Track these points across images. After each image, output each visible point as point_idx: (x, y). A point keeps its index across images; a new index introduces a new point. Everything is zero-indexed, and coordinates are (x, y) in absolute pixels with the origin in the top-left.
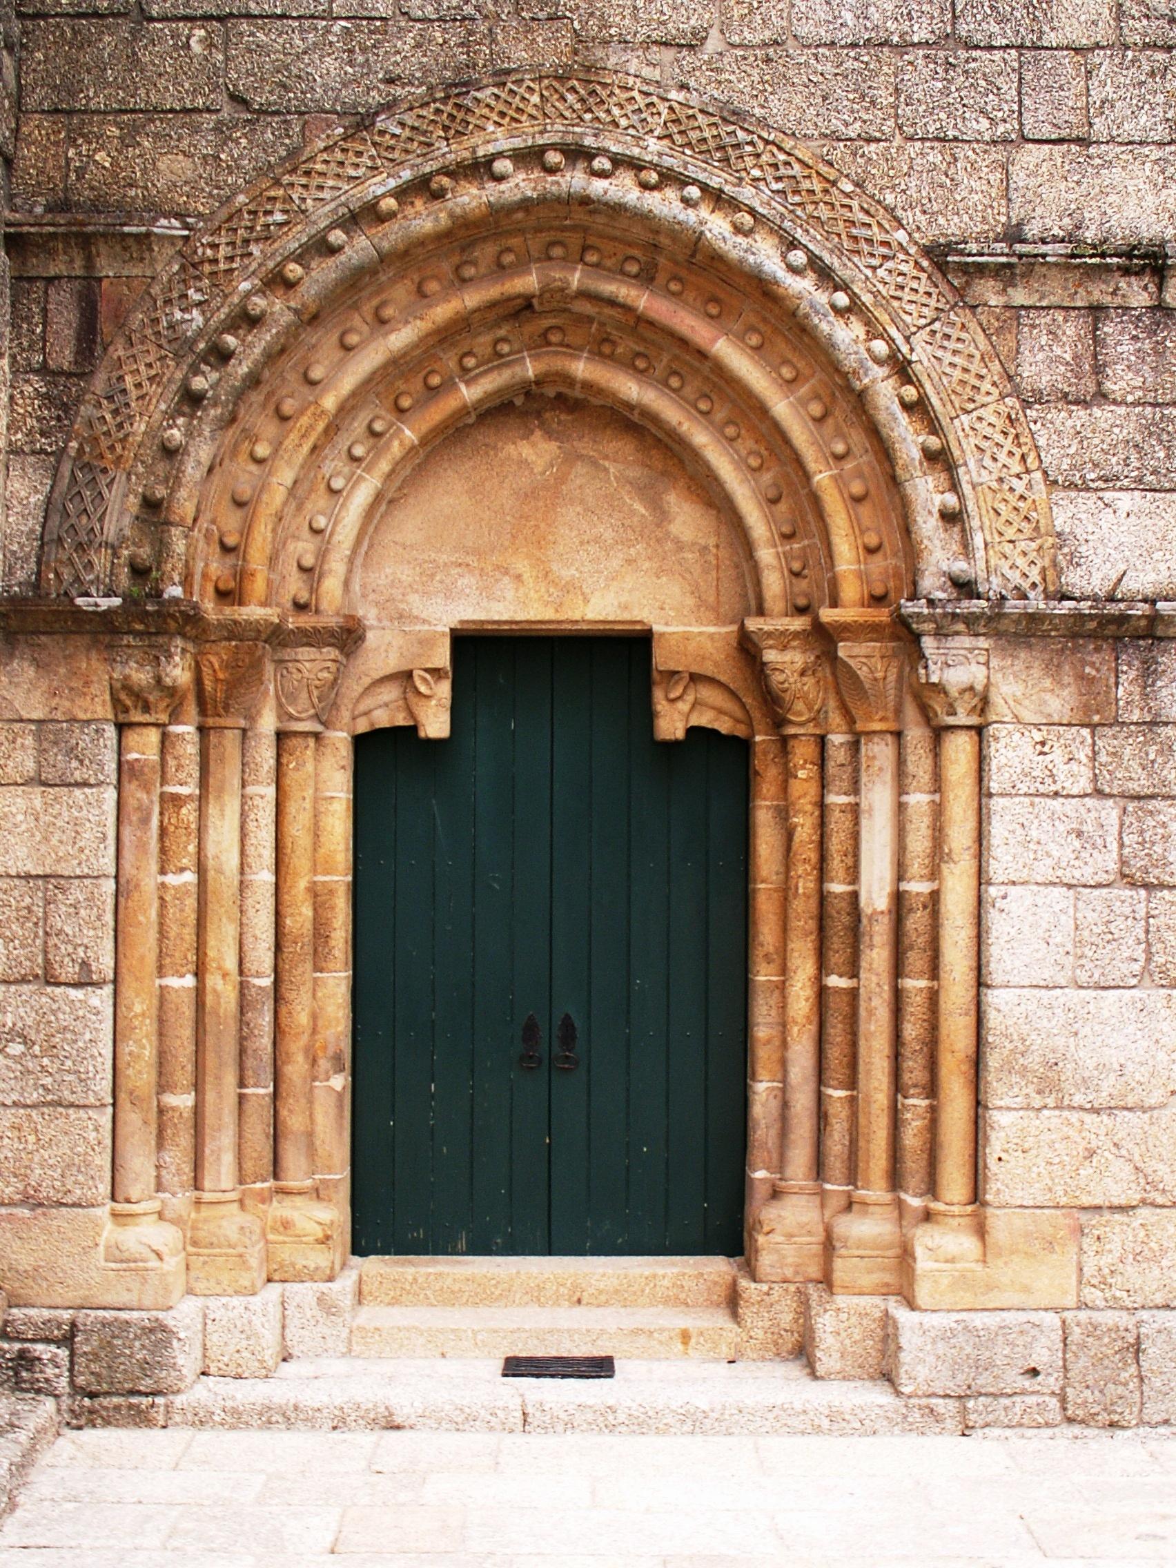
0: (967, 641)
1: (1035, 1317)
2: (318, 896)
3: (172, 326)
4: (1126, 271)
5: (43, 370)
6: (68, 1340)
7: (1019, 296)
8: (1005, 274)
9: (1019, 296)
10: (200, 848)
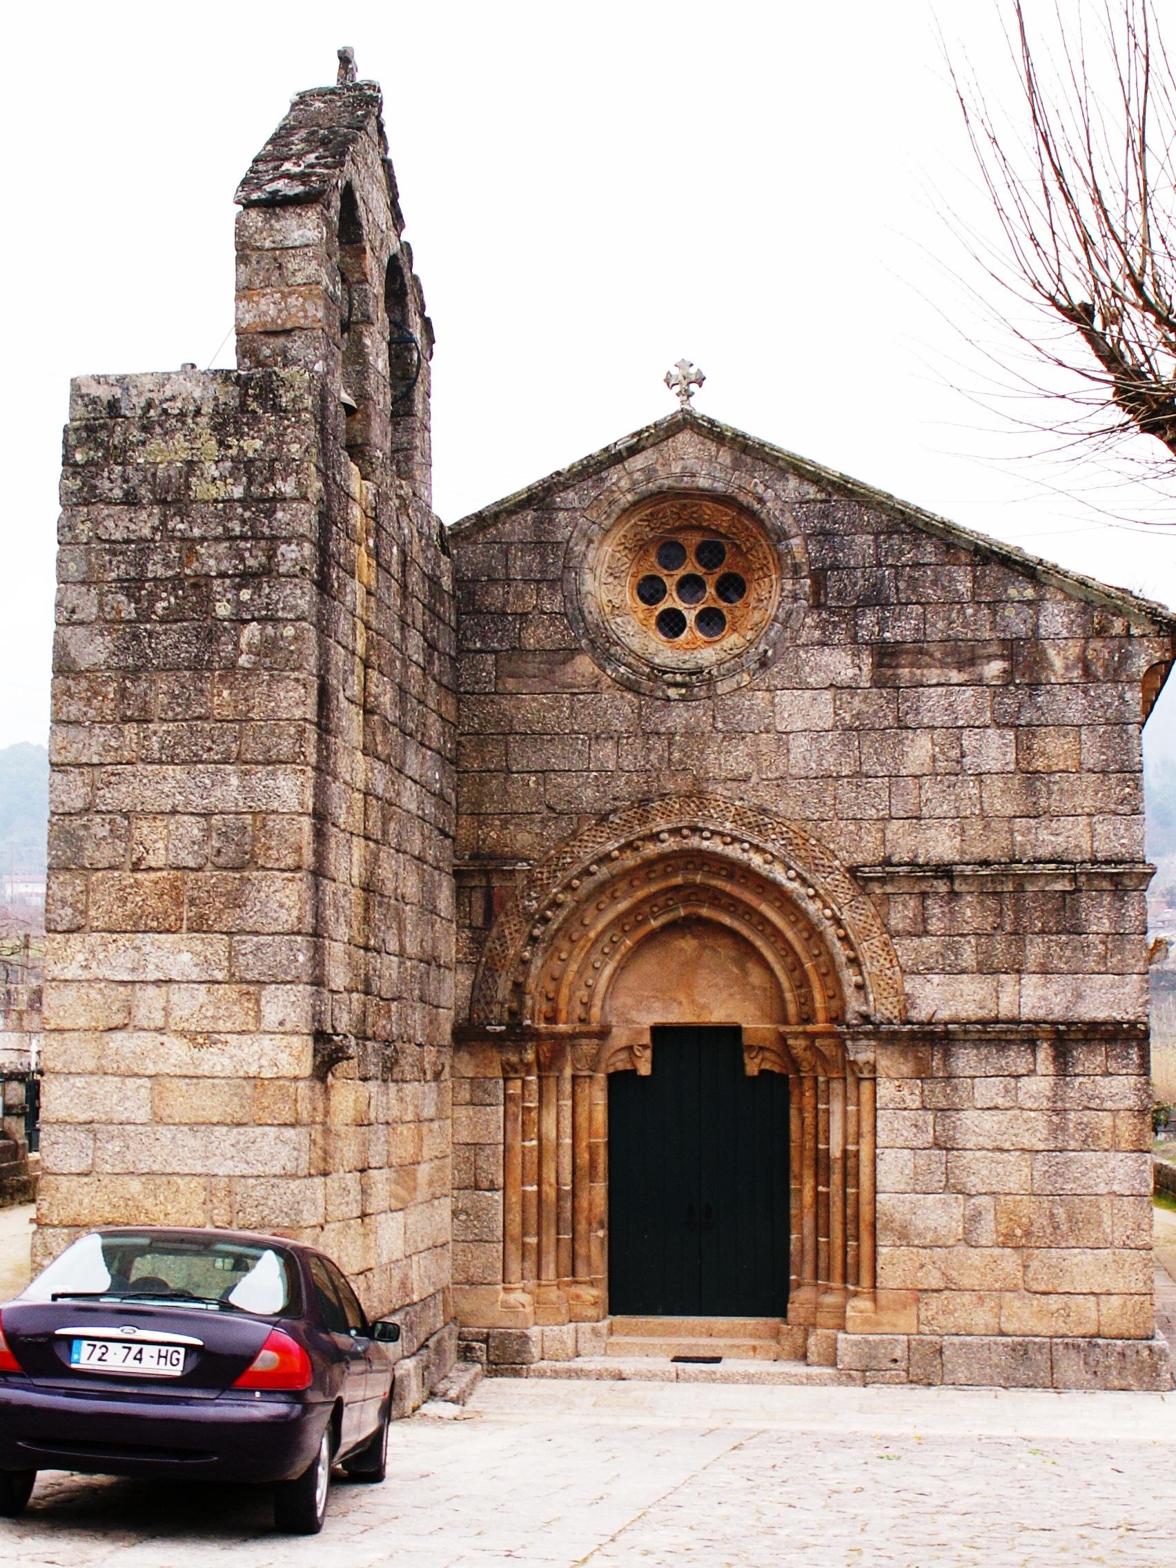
0: (865, 1042)
1: (896, 1337)
2: (591, 1148)
3: (524, 908)
4: (936, 878)
5: (470, 927)
6: (486, 1341)
7: (889, 889)
8: (882, 881)
9: (889, 889)
10: (539, 1130)
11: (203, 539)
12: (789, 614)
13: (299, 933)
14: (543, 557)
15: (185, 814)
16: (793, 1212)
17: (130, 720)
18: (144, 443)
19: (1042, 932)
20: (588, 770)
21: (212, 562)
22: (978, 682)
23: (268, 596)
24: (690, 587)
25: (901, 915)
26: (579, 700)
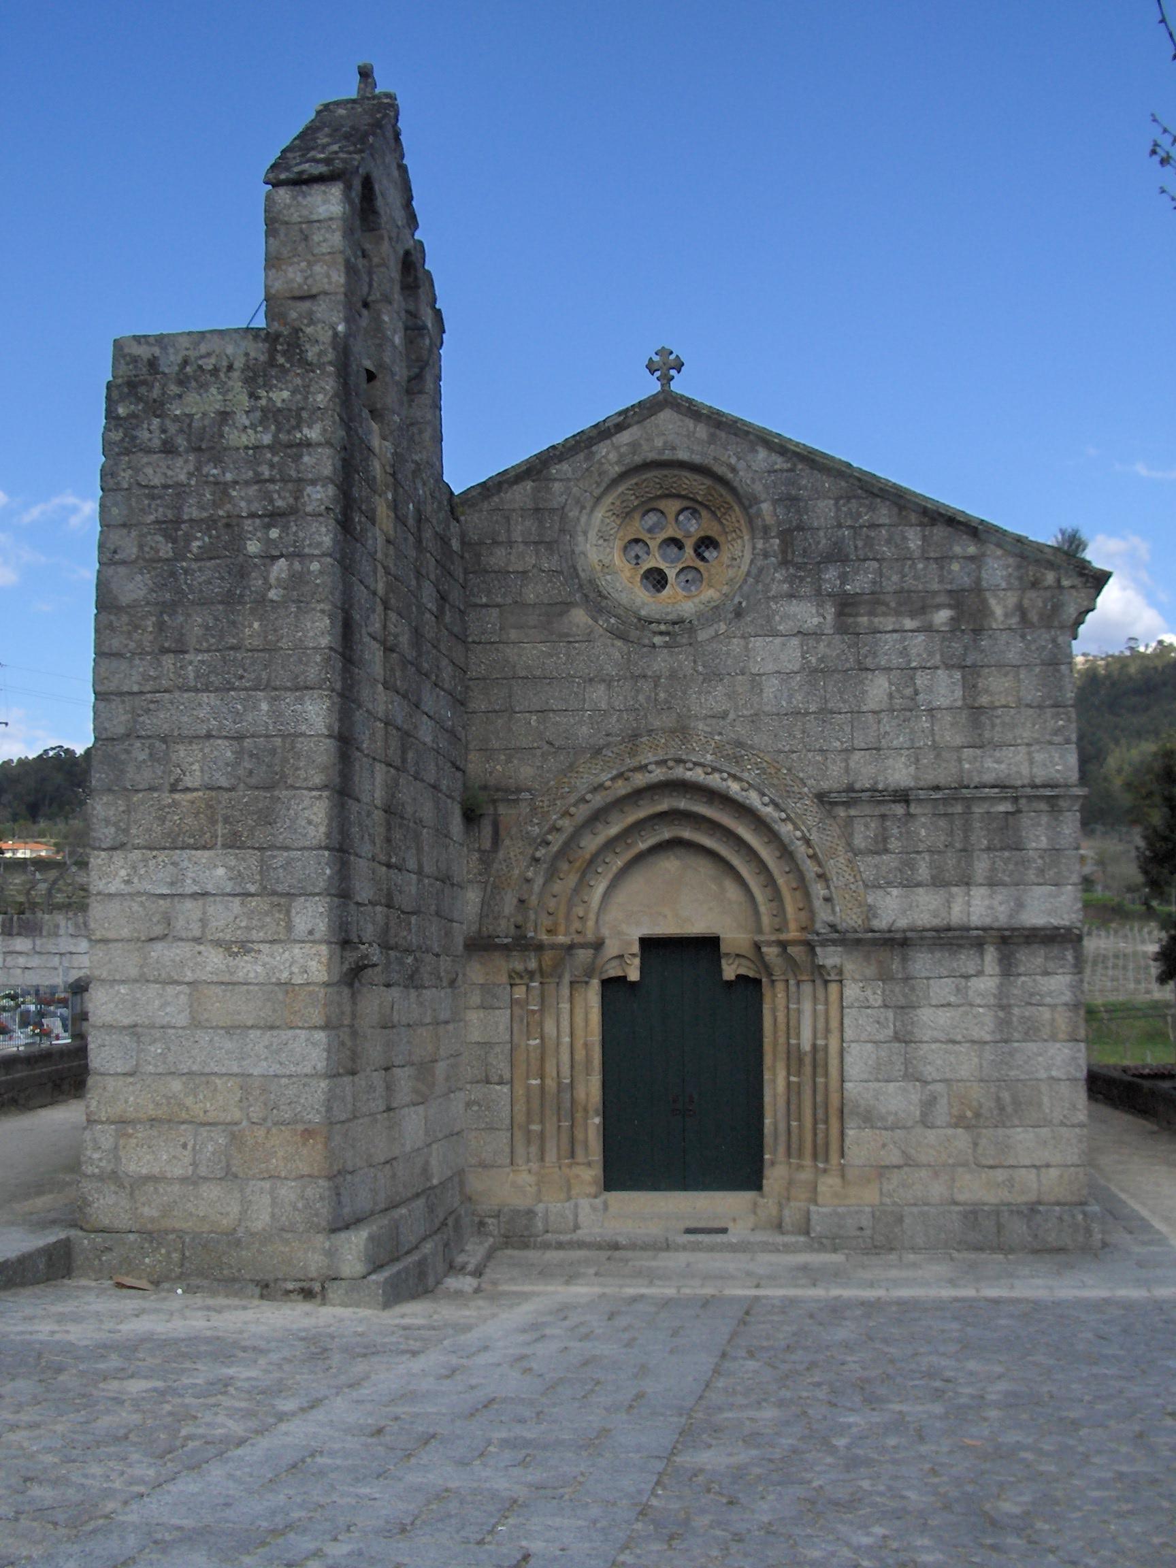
0: (832, 948)
4: (894, 802)
6: (497, 1216)
8: (847, 804)
9: (852, 812)
11: (236, 482)
12: (761, 570)
14: (541, 522)
15: (219, 738)
17: (168, 651)
19: (988, 849)
20: (583, 710)
21: (243, 504)
23: (295, 534)
26: (575, 648)
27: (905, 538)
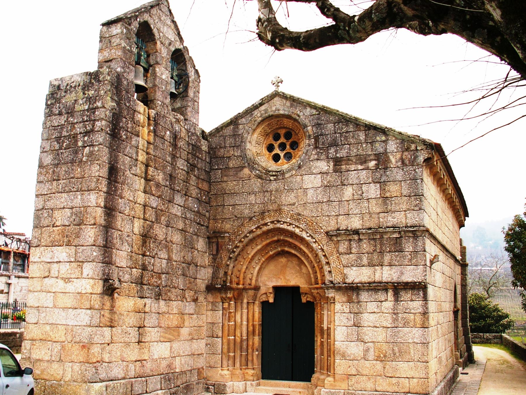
0: (331, 290)
2: (253, 325)
4: (354, 234)
5: (212, 254)
6: (214, 386)
7: (339, 239)
9: (339, 239)
11: (77, 123)
12: (307, 151)
13: (94, 245)
14: (235, 139)
16: (315, 347)
18: (65, 96)
19: (390, 252)
20: (247, 204)
21: (78, 129)
22: (367, 168)
24: (282, 147)
25: (343, 247)
27: (358, 136)
